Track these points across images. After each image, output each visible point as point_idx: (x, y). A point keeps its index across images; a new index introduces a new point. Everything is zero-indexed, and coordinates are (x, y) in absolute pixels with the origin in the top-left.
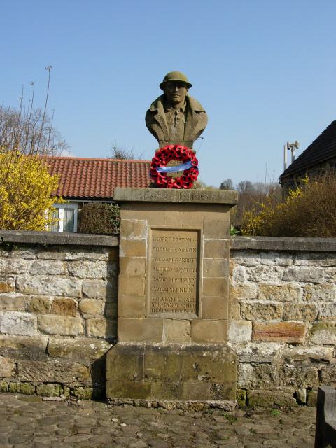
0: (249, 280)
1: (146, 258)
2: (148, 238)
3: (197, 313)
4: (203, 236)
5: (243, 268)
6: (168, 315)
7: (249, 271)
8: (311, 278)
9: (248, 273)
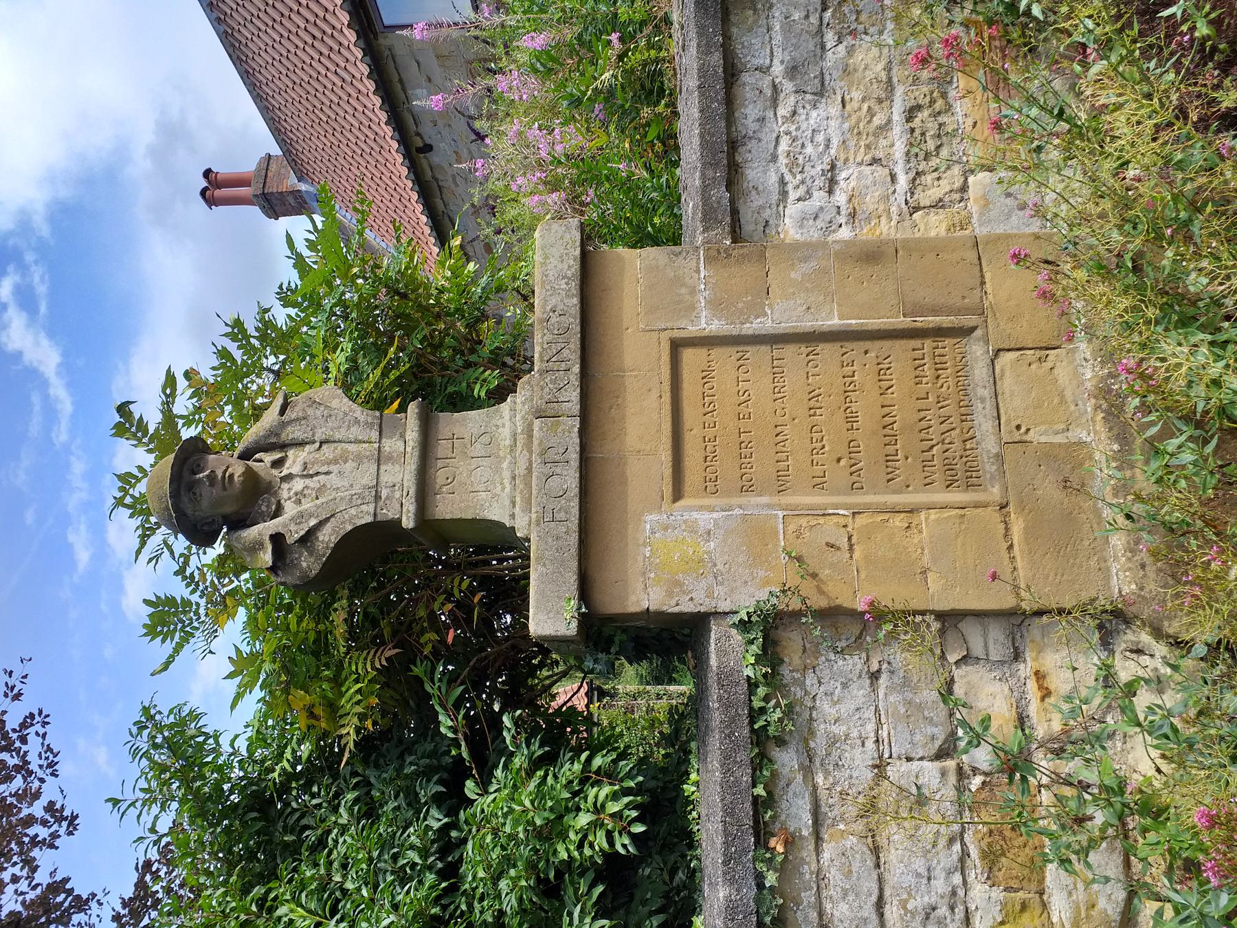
0: (830, 192)
1: (781, 514)
2: (711, 509)
3: (968, 331)
4: (692, 330)
5: (793, 210)
6: (984, 423)
7: (801, 191)
8: (807, 17)
9: (809, 194)
